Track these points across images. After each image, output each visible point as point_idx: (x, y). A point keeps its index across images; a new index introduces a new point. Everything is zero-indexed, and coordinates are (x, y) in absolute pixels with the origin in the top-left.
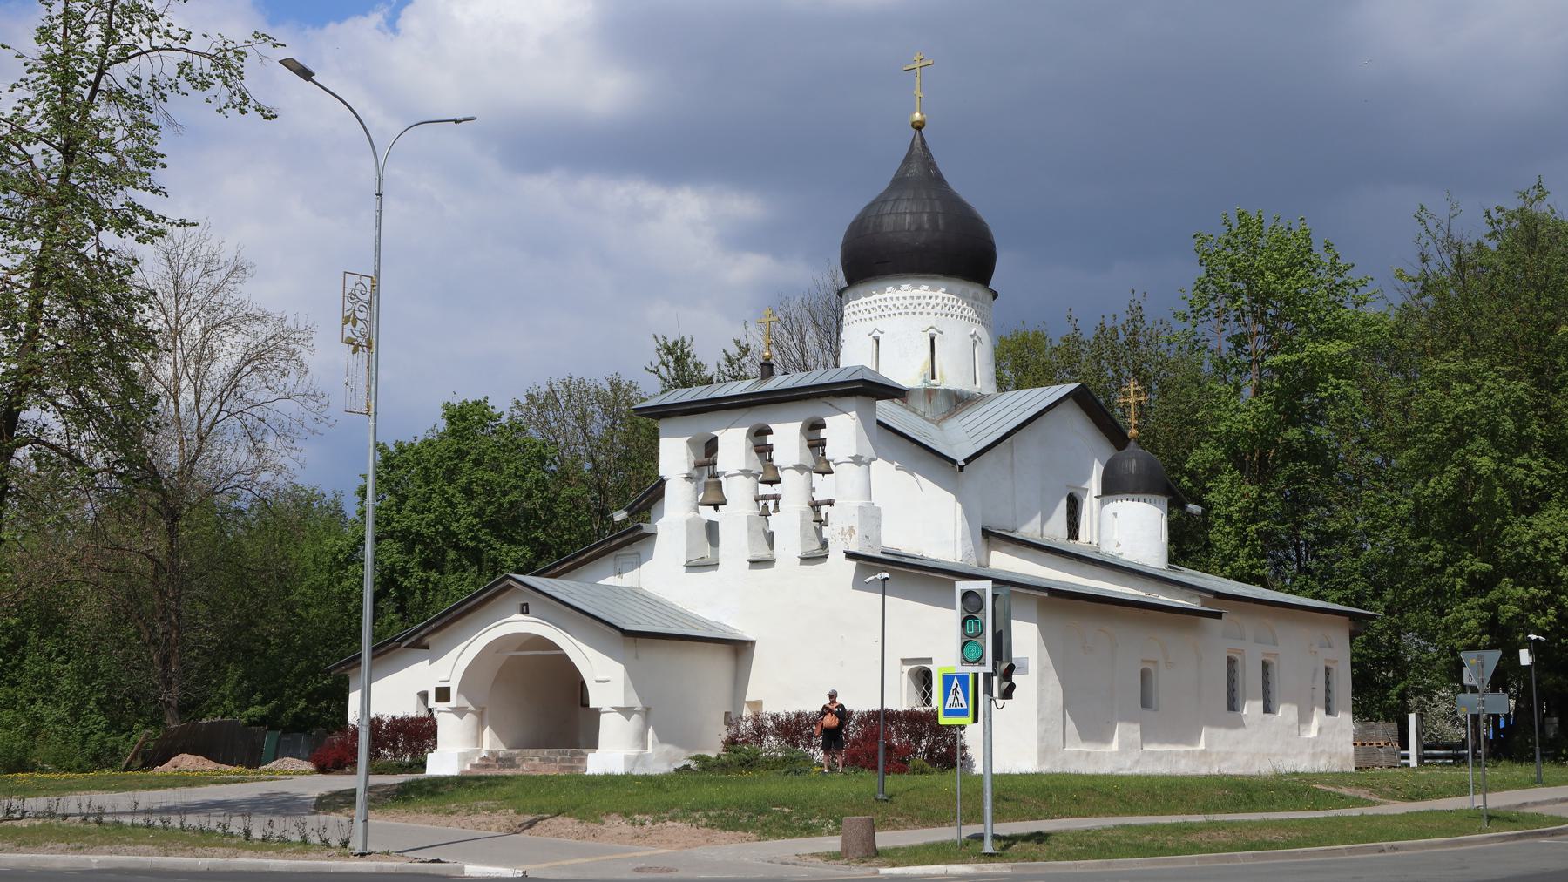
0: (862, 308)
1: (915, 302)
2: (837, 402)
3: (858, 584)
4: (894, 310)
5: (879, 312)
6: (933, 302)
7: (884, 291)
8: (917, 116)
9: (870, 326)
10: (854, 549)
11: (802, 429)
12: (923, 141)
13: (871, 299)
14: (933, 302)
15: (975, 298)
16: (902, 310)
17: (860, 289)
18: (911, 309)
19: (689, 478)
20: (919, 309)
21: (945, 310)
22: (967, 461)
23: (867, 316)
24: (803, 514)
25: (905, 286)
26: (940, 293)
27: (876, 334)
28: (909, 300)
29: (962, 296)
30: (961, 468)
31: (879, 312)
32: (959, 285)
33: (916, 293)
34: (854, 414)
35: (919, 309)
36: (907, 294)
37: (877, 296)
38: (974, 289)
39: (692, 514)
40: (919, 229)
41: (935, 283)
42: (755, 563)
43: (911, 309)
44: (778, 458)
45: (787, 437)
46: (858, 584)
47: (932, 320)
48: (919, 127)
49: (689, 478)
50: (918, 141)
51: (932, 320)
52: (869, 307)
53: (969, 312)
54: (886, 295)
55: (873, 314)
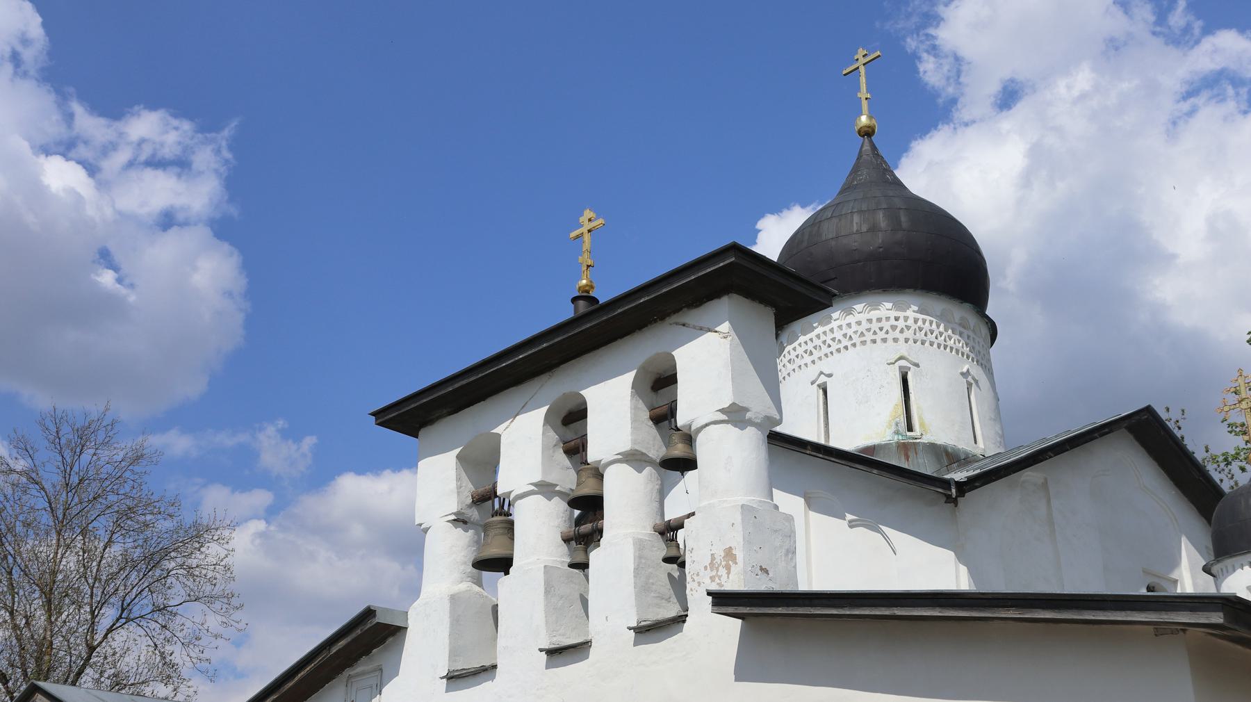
0: (800, 351)
1: (875, 326)
2: (694, 316)
3: (749, 667)
4: (845, 342)
5: (825, 349)
6: (901, 324)
7: (829, 320)
8: (864, 119)
9: (812, 372)
10: (734, 583)
11: (635, 385)
12: (874, 148)
13: (812, 335)
14: (901, 324)
15: (963, 325)
16: (856, 339)
17: (797, 326)
18: (869, 337)
19: (460, 521)
20: (882, 335)
21: (920, 336)
23: (808, 359)
24: (640, 545)
25: (859, 307)
26: (911, 313)
27: (822, 379)
28: (865, 325)
29: (942, 318)
31: (825, 349)
32: (940, 304)
33: (874, 314)
34: (725, 327)
35: (882, 335)
36: (863, 317)
37: (820, 330)
38: (960, 312)
39: (466, 586)
40: (874, 229)
41: (903, 298)
42: (557, 654)
43: (869, 337)
44: (595, 452)
45: (612, 404)
46: (749, 667)
47: (902, 349)
48: (867, 133)
49: (460, 521)
50: (867, 147)
51: (902, 349)
52: (810, 347)
53: (955, 341)
54: (834, 324)
55: (816, 354)
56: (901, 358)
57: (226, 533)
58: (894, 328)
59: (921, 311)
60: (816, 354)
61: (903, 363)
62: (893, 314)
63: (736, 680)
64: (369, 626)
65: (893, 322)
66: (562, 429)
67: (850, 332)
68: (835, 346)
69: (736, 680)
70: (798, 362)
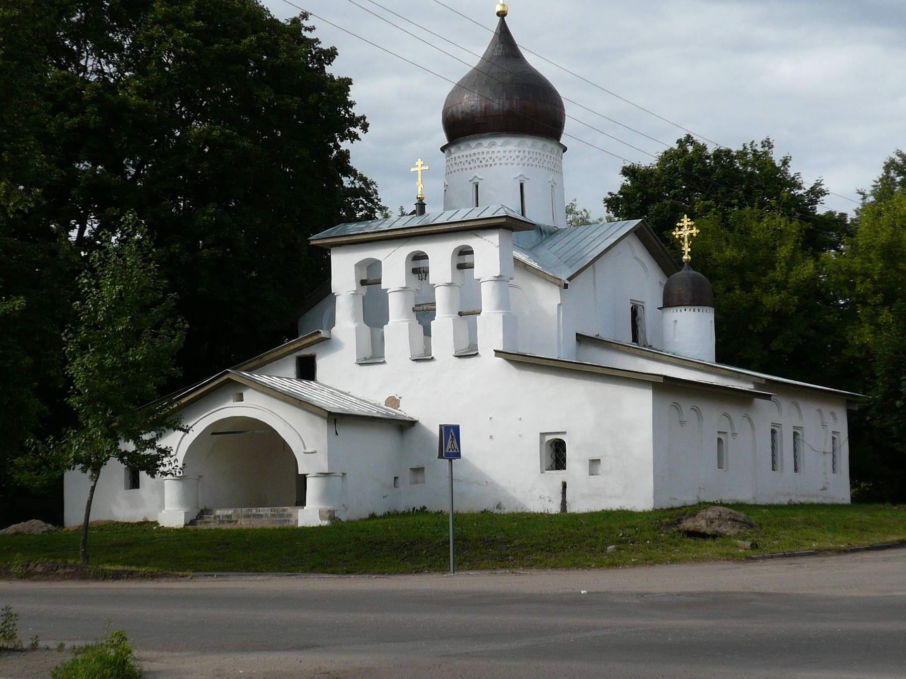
3: (496, 356)
22: (570, 279)
23: (468, 166)
27: (476, 180)
30: (566, 286)
35: (511, 160)
38: (550, 145)
43: (504, 161)
55: (472, 164)
56: (521, 175)
57: (164, 428)
58: (518, 157)
59: (518, 146)
60: (472, 164)
61: (522, 178)
62: (518, 149)
63: (565, 469)
64: (711, 623)
65: (517, 153)
66: (456, 257)
67: (494, 156)
68: (484, 162)
69: (565, 469)
70: (461, 166)
